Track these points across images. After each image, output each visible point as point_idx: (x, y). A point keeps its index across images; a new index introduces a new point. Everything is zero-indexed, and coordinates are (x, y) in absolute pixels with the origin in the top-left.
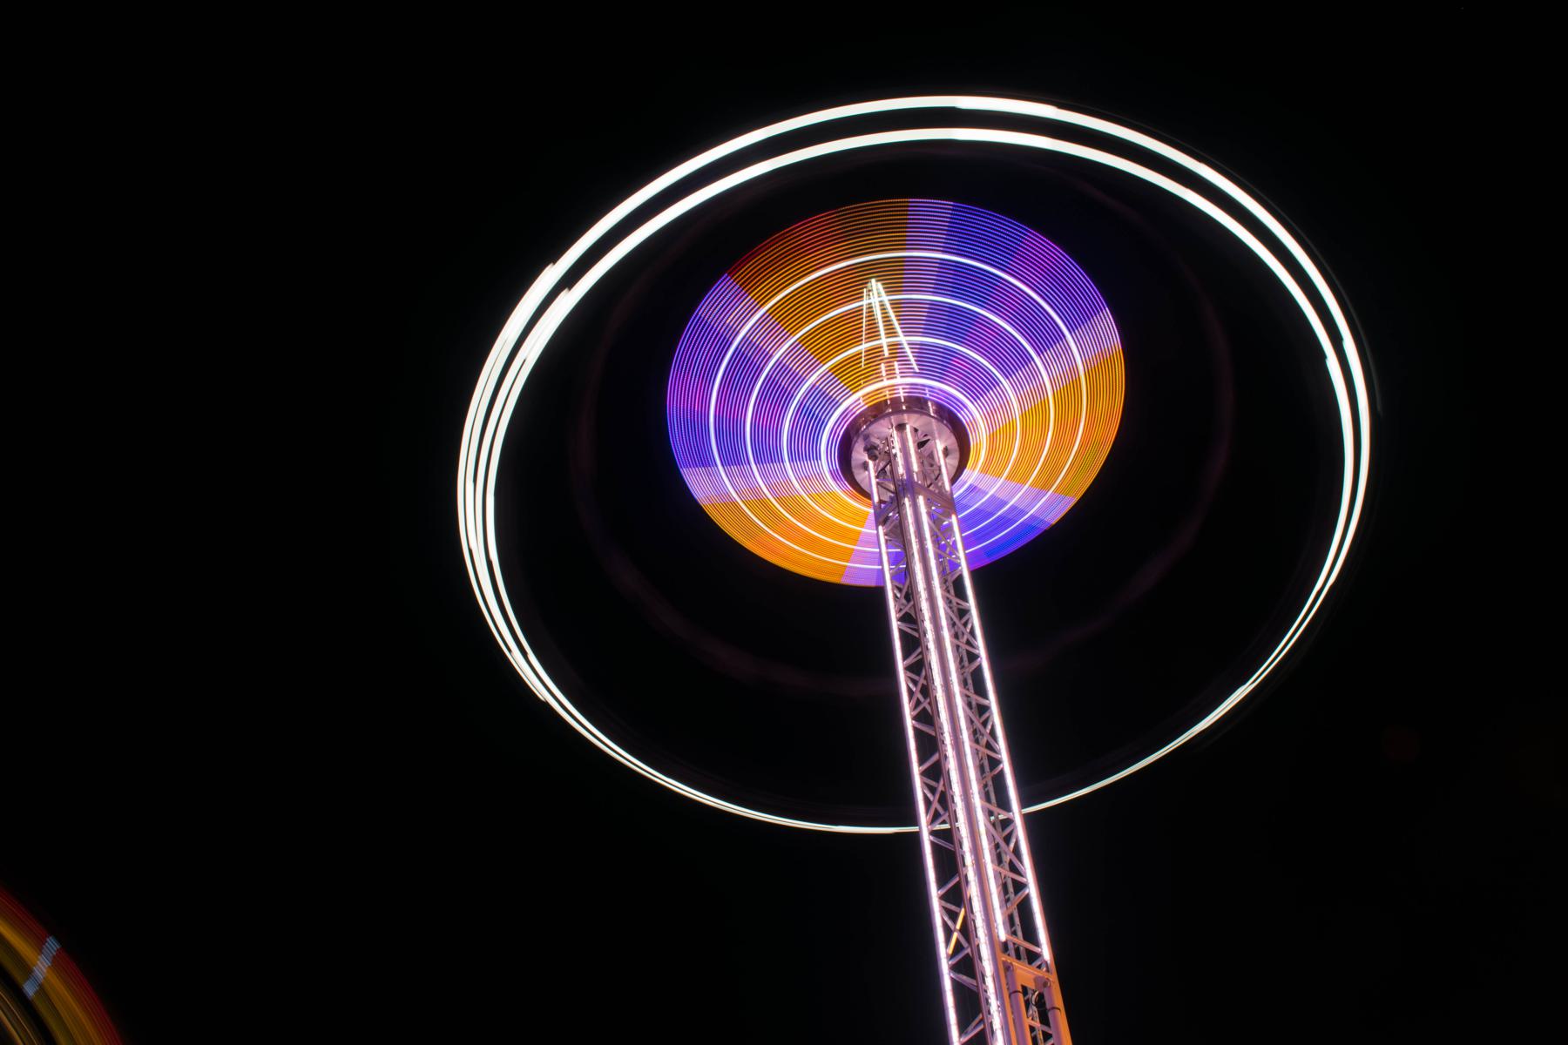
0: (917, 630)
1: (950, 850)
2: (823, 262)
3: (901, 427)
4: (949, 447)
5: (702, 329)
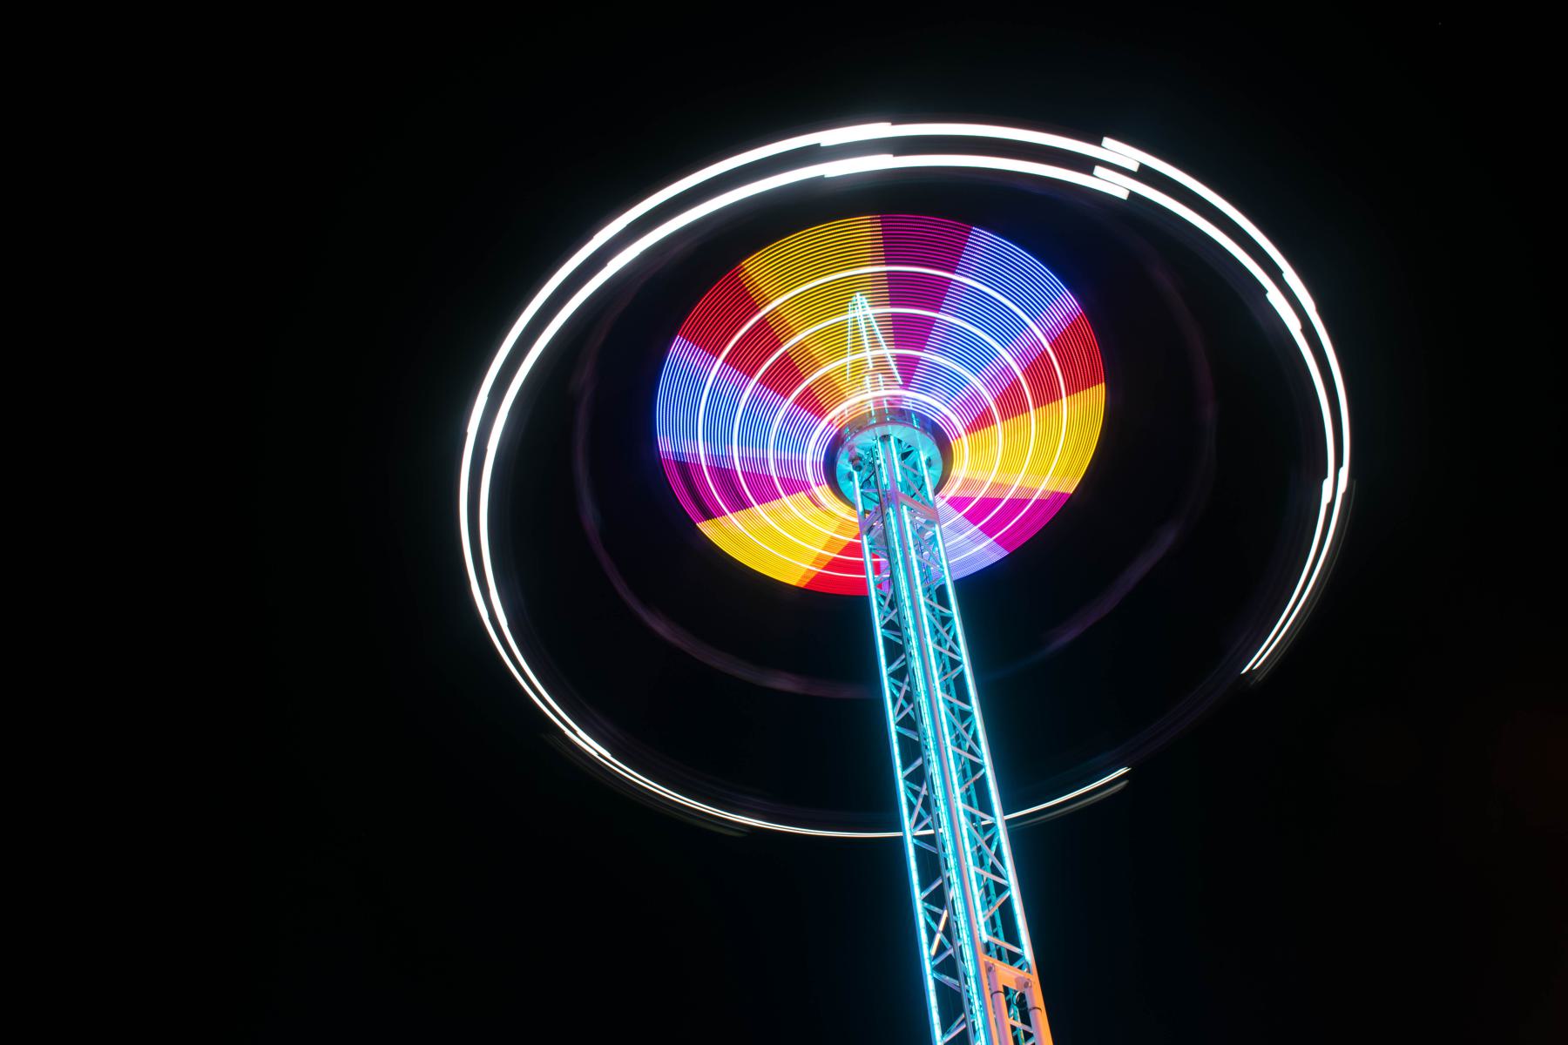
0: (900, 638)
2: (985, 262)
4: (847, 481)
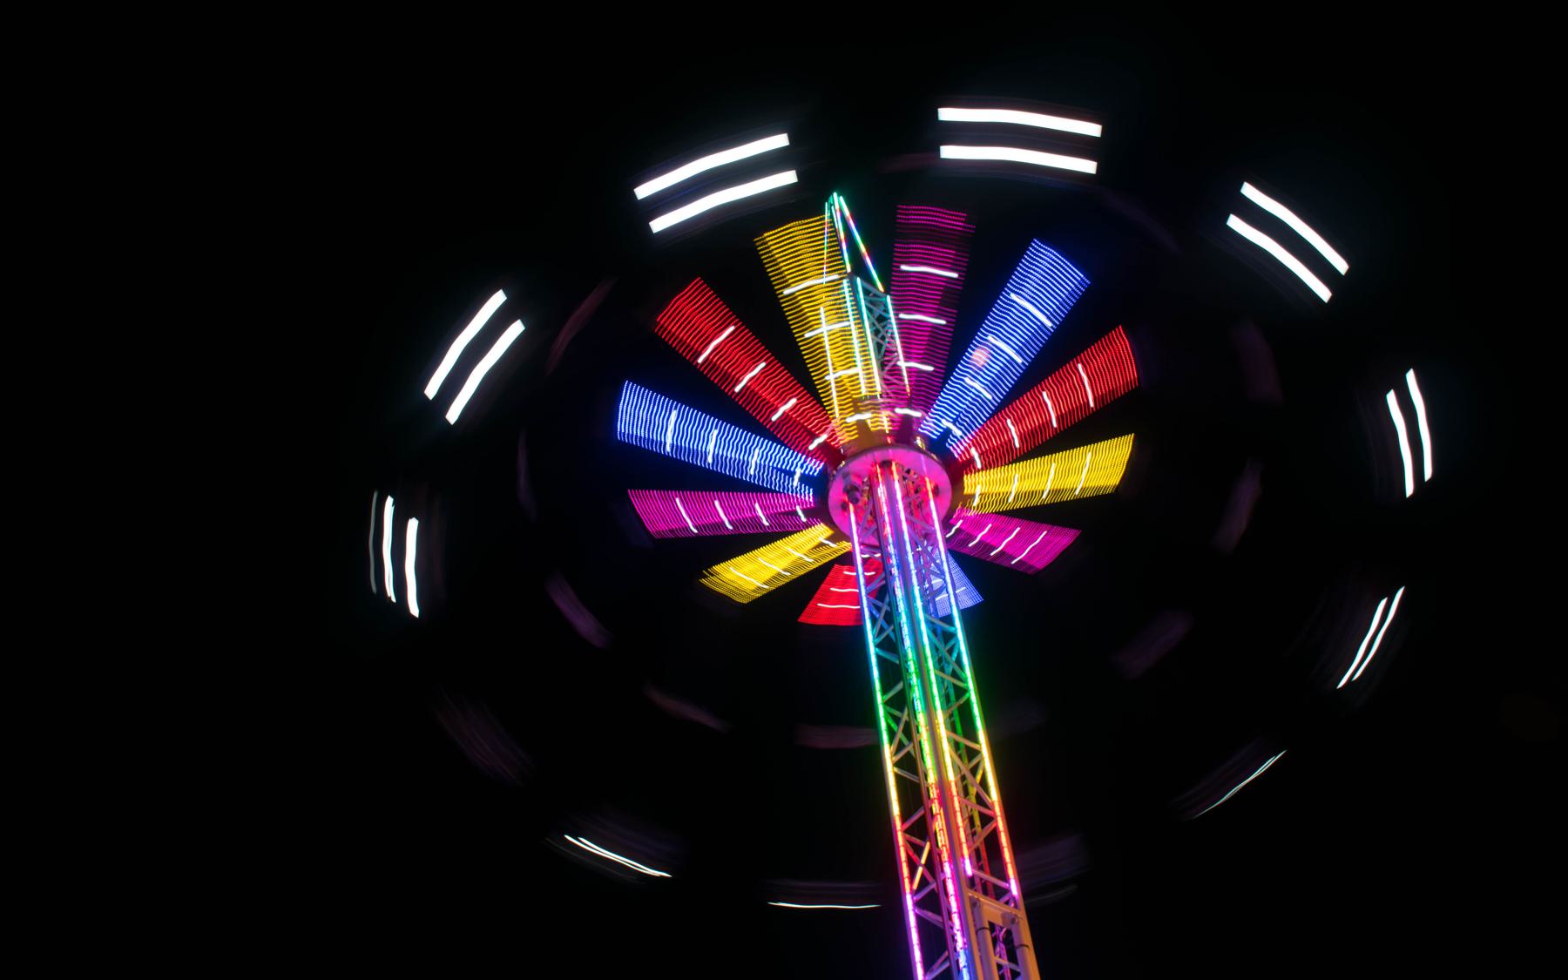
1: (896, 664)
3: (886, 465)
5: (1005, 336)
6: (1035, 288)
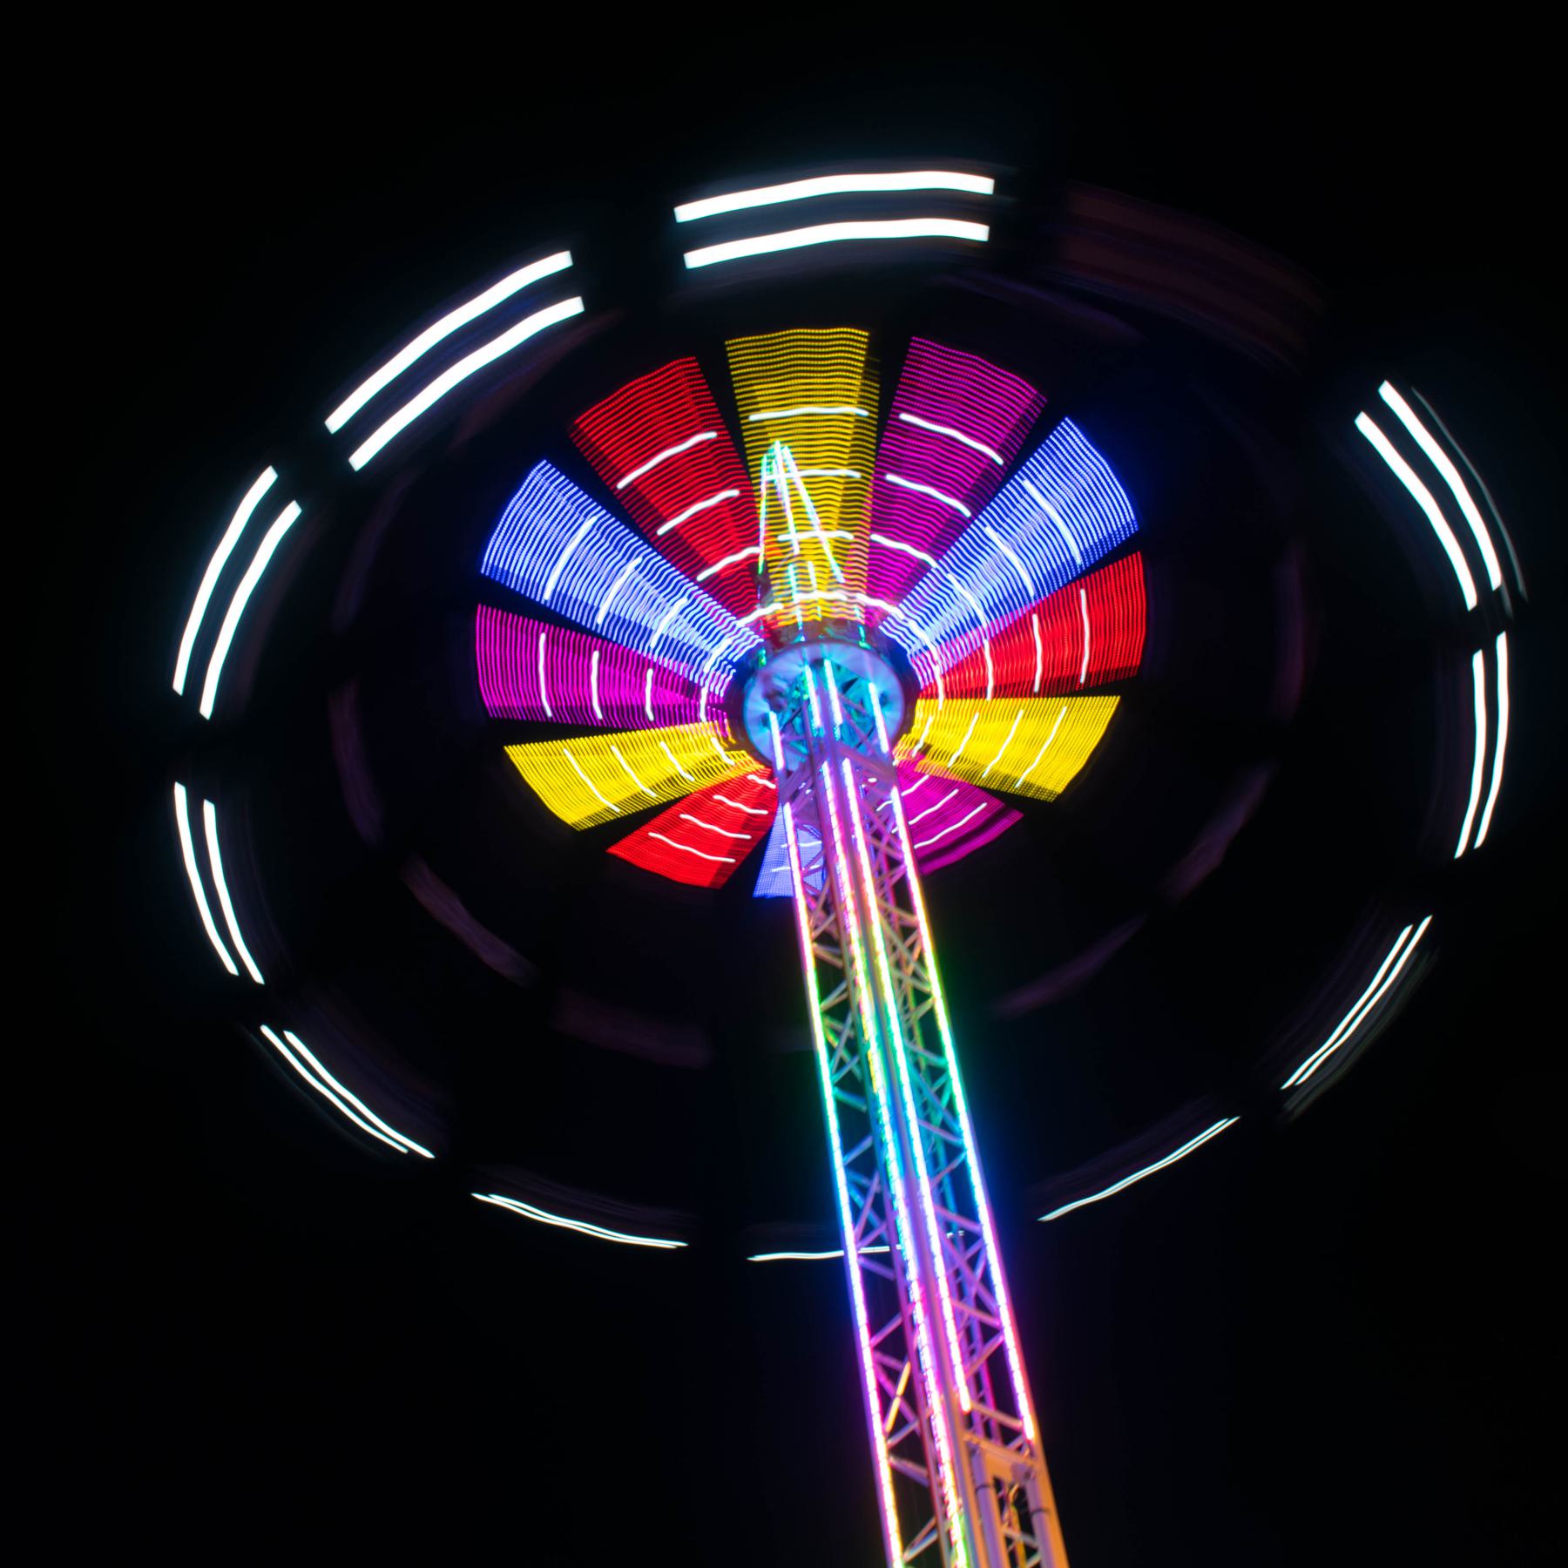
6: (671, 410)
